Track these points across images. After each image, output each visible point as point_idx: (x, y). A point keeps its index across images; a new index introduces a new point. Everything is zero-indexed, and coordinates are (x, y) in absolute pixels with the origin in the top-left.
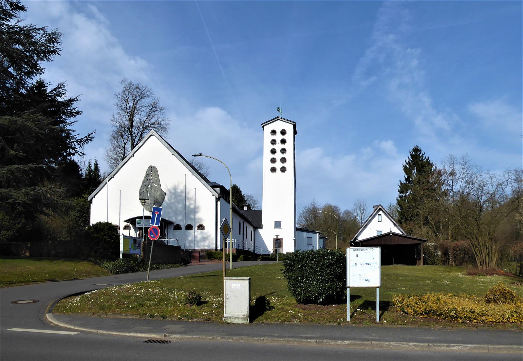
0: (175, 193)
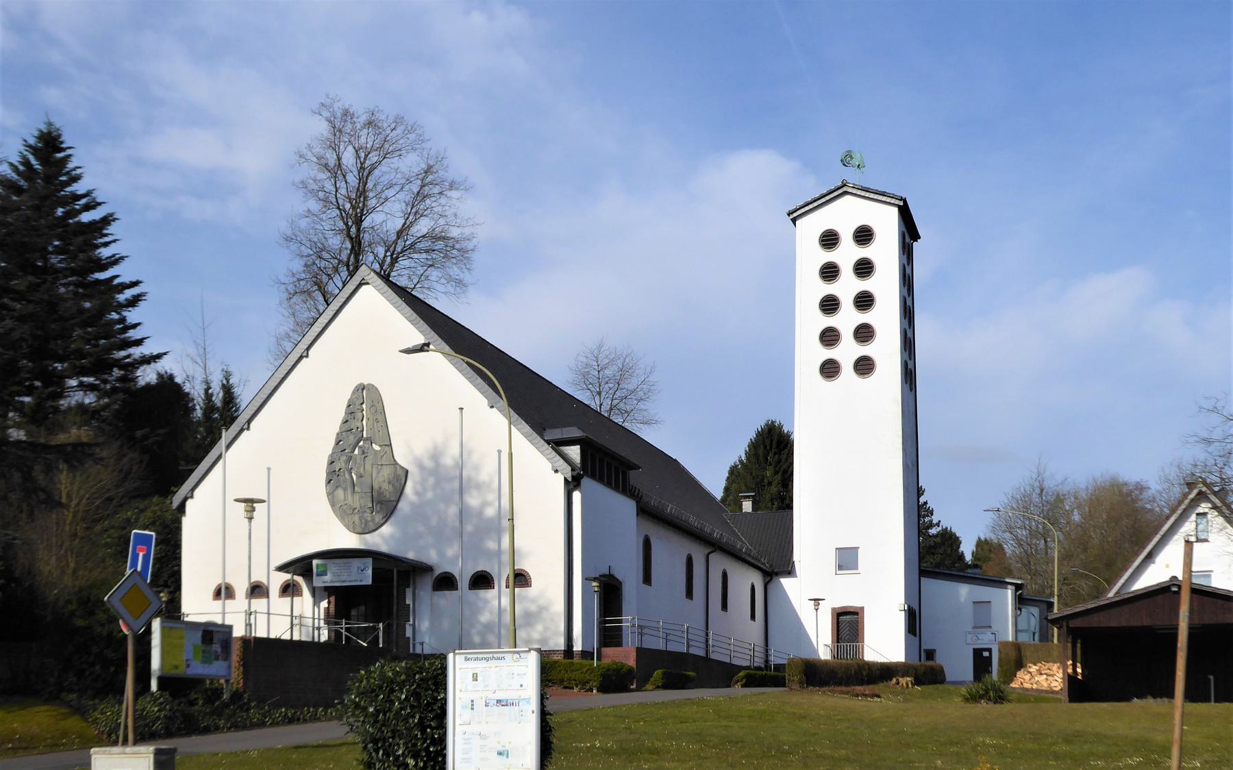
0: (434, 469)
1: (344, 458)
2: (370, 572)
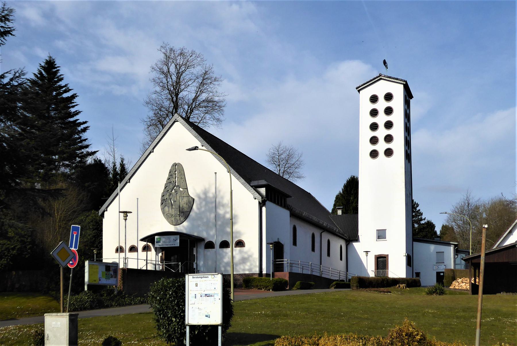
0: (205, 198)
1: (168, 194)
2: (178, 241)
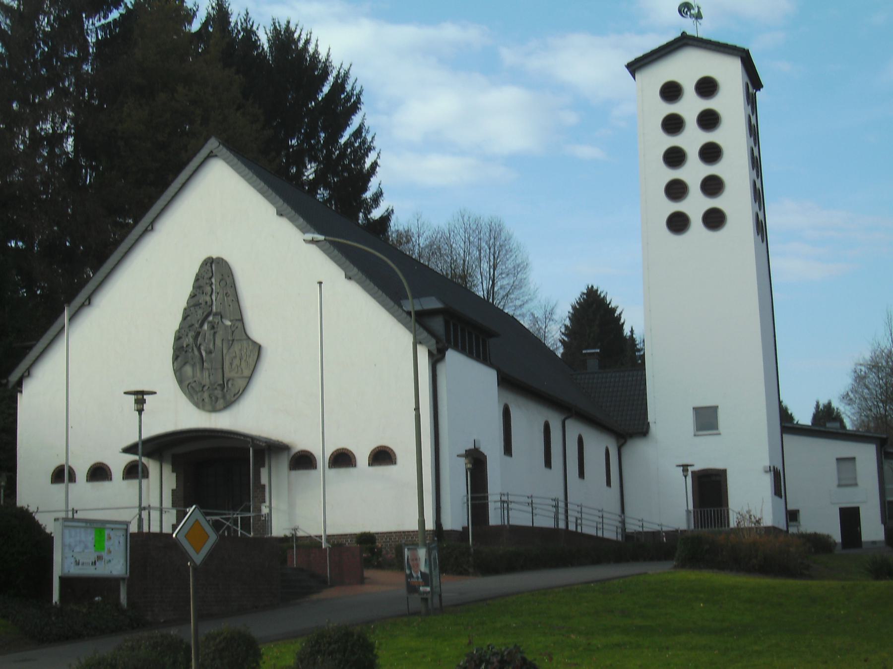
1: (191, 334)
